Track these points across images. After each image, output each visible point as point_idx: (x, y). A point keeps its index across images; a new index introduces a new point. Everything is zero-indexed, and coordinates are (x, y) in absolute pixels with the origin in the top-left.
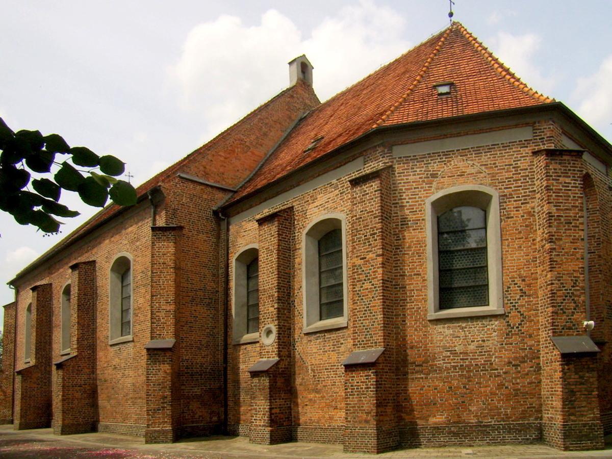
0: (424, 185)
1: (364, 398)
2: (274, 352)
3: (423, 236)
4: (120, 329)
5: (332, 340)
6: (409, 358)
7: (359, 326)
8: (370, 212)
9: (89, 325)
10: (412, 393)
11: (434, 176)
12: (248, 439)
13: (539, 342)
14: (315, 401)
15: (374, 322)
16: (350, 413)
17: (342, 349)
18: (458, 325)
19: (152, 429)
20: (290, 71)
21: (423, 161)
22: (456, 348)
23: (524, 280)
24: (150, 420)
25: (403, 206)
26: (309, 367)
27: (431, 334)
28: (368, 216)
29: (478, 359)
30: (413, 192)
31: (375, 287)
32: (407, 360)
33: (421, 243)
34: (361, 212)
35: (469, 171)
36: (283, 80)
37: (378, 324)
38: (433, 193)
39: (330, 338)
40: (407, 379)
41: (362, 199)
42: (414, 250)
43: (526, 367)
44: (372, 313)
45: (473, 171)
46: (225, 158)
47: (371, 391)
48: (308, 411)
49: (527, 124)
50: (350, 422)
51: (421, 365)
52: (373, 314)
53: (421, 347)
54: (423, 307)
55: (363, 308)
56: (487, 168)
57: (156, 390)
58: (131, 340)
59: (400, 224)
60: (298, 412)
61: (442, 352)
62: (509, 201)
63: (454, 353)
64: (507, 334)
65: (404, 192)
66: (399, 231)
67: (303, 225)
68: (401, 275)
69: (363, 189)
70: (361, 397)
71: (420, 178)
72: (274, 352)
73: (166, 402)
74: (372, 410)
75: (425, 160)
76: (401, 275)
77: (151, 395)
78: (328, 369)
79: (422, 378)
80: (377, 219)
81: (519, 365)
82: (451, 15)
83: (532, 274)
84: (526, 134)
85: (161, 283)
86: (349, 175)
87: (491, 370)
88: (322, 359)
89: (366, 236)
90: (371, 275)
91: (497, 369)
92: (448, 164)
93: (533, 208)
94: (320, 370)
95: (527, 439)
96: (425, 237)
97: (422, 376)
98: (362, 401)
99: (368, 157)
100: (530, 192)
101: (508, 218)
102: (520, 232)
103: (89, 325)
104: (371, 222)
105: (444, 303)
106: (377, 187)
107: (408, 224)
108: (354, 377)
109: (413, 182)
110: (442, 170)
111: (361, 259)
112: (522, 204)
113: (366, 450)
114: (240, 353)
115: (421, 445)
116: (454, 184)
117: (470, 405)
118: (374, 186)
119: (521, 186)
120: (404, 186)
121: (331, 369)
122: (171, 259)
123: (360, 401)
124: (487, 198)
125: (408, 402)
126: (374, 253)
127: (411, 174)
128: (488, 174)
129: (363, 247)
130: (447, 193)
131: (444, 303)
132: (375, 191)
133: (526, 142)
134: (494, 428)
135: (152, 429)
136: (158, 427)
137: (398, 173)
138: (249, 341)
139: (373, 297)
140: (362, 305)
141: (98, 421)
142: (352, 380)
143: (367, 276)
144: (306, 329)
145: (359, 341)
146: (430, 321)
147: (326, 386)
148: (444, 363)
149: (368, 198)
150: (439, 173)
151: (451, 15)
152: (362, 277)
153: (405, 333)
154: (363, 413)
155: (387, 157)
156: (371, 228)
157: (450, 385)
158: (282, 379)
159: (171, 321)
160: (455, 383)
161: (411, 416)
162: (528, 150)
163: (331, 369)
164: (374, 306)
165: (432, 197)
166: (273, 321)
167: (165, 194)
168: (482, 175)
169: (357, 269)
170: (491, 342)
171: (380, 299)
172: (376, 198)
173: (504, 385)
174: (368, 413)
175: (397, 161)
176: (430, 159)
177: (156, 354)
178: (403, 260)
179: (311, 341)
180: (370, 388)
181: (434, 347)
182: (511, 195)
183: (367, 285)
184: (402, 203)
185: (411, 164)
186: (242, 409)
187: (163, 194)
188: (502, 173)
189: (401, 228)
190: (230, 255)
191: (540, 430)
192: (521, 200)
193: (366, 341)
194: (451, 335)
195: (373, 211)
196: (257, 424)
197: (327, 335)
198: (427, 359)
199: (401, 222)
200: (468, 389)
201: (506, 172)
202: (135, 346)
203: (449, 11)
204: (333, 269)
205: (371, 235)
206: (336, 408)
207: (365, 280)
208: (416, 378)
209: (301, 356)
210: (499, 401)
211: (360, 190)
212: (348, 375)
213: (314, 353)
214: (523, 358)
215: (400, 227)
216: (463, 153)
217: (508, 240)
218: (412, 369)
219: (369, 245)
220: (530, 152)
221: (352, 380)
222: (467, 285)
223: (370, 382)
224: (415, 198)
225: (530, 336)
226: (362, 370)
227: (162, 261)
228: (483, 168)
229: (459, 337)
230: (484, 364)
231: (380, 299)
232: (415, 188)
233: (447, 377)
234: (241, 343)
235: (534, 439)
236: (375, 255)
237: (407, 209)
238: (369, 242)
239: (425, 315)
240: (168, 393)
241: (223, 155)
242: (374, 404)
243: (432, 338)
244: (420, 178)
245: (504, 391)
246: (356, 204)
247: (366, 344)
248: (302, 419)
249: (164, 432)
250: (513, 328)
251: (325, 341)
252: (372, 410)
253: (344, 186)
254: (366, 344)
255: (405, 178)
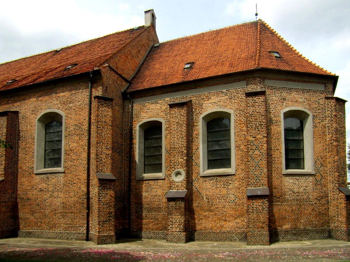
0: (280, 103)
1: (260, 214)
2: (183, 186)
3: (280, 129)
4: (44, 163)
5: (223, 181)
6: (274, 193)
7: (252, 175)
8: (259, 112)
9: (12, 158)
10: (275, 212)
11: (284, 99)
12: (165, 240)
13: (328, 189)
14: (209, 217)
15: (262, 173)
16: (252, 223)
17: (231, 186)
18: (295, 178)
19: (102, 234)
20: (145, 16)
21: (279, 90)
22: (295, 190)
23: (322, 158)
24: (101, 228)
25: (270, 112)
26: (205, 197)
27: (284, 182)
28: (257, 114)
29: (304, 196)
30: (275, 106)
31: (262, 154)
32: (273, 195)
33: (279, 133)
34: (252, 111)
35: (300, 100)
36: (140, 21)
37: (264, 174)
38: (284, 108)
39: (222, 180)
40: (273, 205)
41: (253, 104)
42: (276, 137)
43: (323, 201)
44: (260, 168)
45: (301, 101)
46: (125, 61)
47: (265, 211)
48: (203, 222)
49: (323, 83)
50: (251, 228)
51: (279, 198)
52: (261, 168)
53: (279, 188)
54: (280, 167)
55: (254, 164)
56: (307, 100)
57: (105, 208)
58: (63, 171)
59: (269, 121)
60: (195, 223)
61: (289, 191)
62: (316, 119)
63: (293, 192)
64: (316, 185)
65: (271, 105)
66: (269, 125)
67: (200, 112)
68: (270, 149)
69: (254, 99)
70: (259, 214)
71: (278, 99)
72: (183, 186)
73: (112, 216)
74: (266, 221)
75: (280, 90)
76: (270, 149)
77: (101, 211)
78: (220, 198)
79: (280, 205)
80: (263, 117)
81: (320, 200)
82: (256, 15)
83: (325, 156)
84: (321, 88)
85: (103, 135)
86: (235, 89)
87: (310, 202)
88: (215, 192)
89: (256, 125)
90: (259, 147)
91: (312, 202)
92: (291, 95)
93: (326, 124)
94: (213, 198)
95: (324, 237)
96: (281, 131)
97: (280, 203)
98: (260, 216)
99: (250, 82)
100: (324, 116)
101: (316, 127)
102: (320, 135)
103: (12, 158)
104: (259, 118)
105: (287, 167)
106: (263, 100)
107: (272, 122)
108: (254, 203)
109: (275, 100)
110: (288, 97)
111: (253, 137)
112: (321, 121)
113: (262, 244)
114: (143, 186)
115: (279, 240)
116: (293, 106)
117: (300, 219)
118: (260, 99)
119: (321, 113)
120: (271, 102)
121: (222, 198)
122: (110, 120)
123: (258, 216)
124: (306, 115)
125: (273, 217)
126: (261, 135)
127: (274, 96)
128: (308, 104)
129: (254, 131)
130: (291, 110)
131: (287, 167)
132: (262, 102)
133: (322, 92)
134: (311, 231)
135: (102, 234)
136: (106, 233)
137: (268, 94)
138: (149, 179)
139: (261, 159)
140: (254, 163)
141: (18, 228)
142: (253, 204)
143: (257, 147)
144: (202, 173)
145: (252, 183)
146: (283, 175)
147: (218, 208)
148: (290, 197)
149: (257, 105)
150: (287, 98)
151: (256, 15)
152: (254, 148)
153: (272, 180)
154: (260, 223)
155: (262, 84)
156: (259, 121)
157: (292, 209)
158: (187, 203)
159: (109, 161)
160: (294, 208)
161: (275, 225)
162: (323, 96)
163: (222, 198)
164: (262, 164)
165: (284, 110)
166: (182, 167)
167: (103, 76)
168: (305, 104)
169: (250, 143)
170: (309, 187)
171: (265, 161)
172: (262, 105)
173: (315, 209)
174: (263, 223)
175: (267, 88)
176: (282, 90)
177: (106, 183)
178: (271, 141)
179: (206, 181)
180: (265, 209)
181: (285, 188)
182: (317, 116)
183: (257, 152)
184: (270, 110)
185: (274, 91)
186: (144, 221)
187: (101, 75)
188: (313, 104)
189: (270, 124)
190: (134, 123)
191: (330, 232)
192: (320, 119)
193: (256, 183)
194: (292, 182)
195: (260, 112)
196: (173, 230)
197: (219, 178)
198: (282, 195)
199: (270, 120)
200: (299, 211)
201: (315, 104)
202: (65, 176)
203: (256, 13)
204: (217, 140)
205: (259, 125)
206: (226, 221)
207: (256, 149)
208: (277, 204)
209: (197, 190)
210: (313, 217)
211: (252, 99)
212: (250, 201)
213: (209, 188)
214: (322, 196)
215: (269, 123)
216: (297, 90)
217: (315, 138)
218: (275, 200)
219: (258, 130)
220: (324, 97)
221: (253, 204)
222: (294, 158)
223: (265, 206)
224: (276, 109)
225: (325, 186)
226: (259, 199)
227: (103, 120)
228: (305, 100)
229: (296, 184)
230: (307, 199)
231: (265, 161)
232: (276, 104)
233: (291, 205)
234: (144, 179)
235: (327, 236)
236: (262, 136)
237: (273, 114)
238: (258, 129)
239: (281, 171)
240: (112, 210)
241: (123, 58)
242: (267, 218)
243: (284, 183)
244: (278, 99)
245: (315, 213)
246: (249, 106)
247: (256, 185)
248: (198, 227)
249: (110, 237)
250: (318, 181)
251: (217, 182)
252: (266, 221)
253: (232, 95)
254: (256, 185)
255: (271, 97)
